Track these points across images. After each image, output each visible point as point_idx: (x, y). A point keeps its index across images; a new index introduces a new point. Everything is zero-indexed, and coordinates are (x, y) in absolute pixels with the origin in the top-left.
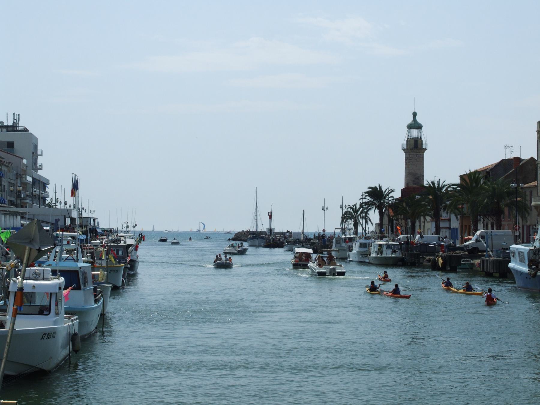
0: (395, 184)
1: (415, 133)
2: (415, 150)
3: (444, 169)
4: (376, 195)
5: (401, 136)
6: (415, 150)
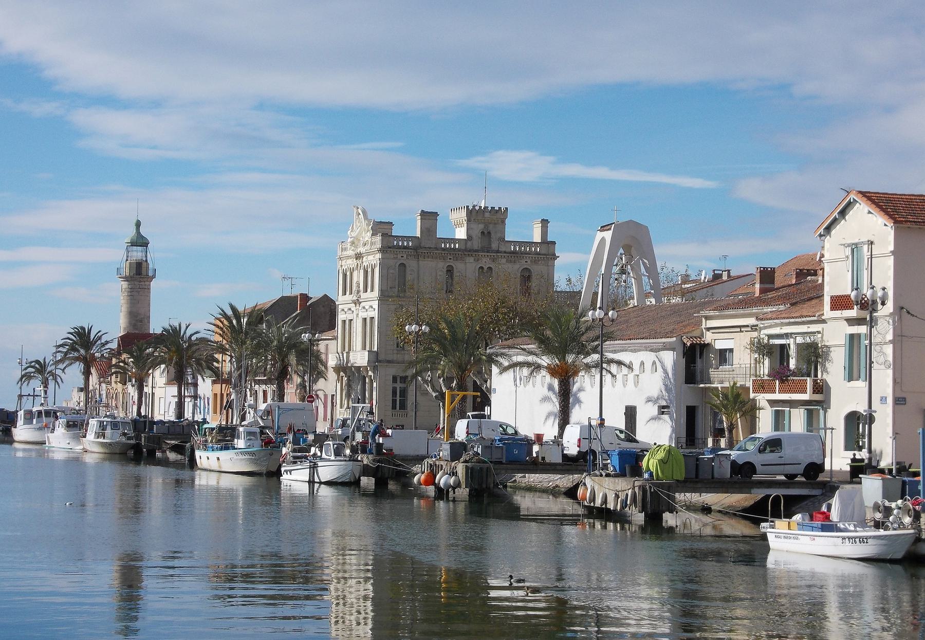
0: (112, 326)
1: (137, 254)
2: (139, 276)
3: (187, 305)
4: (82, 344)
5: (117, 255)
6: (139, 276)
